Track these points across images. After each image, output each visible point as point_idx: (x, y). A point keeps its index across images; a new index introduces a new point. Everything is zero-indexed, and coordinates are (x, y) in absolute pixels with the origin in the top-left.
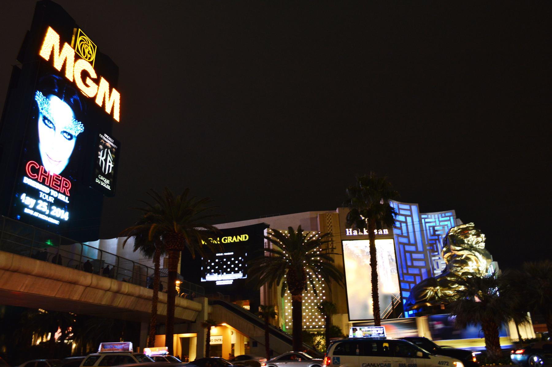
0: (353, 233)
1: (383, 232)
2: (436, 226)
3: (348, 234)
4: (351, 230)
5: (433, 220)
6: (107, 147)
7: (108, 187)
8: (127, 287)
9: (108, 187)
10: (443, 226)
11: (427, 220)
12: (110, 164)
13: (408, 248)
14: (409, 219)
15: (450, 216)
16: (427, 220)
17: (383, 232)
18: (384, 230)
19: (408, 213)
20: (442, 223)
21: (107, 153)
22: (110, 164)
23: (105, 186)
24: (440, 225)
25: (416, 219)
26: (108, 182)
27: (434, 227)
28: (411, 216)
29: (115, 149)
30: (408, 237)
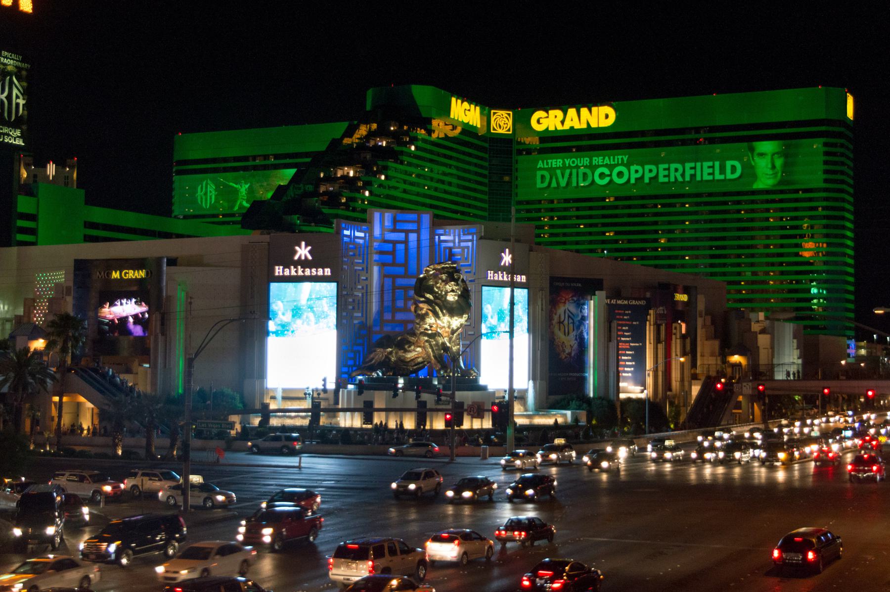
0: (283, 272)
1: (324, 272)
2: (454, 247)
3: (277, 274)
4: (281, 267)
5: (450, 238)
6: (10, 74)
7: (20, 142)
8: (211, 188)
9: (20, 142)
10: (463, 248)
11: (442, 238)
12: (18, 101)
13: (400, 281)
14: (413, 237)
15: (472, 234)
16: (442, 238)
17: (324, 272)
18: (326, 270)
19: (413, 226)
20: (463, 244)
21: (11, 83)
22: (18, 101)
23: (12, 141)
24: (459, 247)
25: (425, 235)
26: (18, 133)
27: (450, 249)
28: (418, 231)
29: (26, 70)
30: (406, 265)
